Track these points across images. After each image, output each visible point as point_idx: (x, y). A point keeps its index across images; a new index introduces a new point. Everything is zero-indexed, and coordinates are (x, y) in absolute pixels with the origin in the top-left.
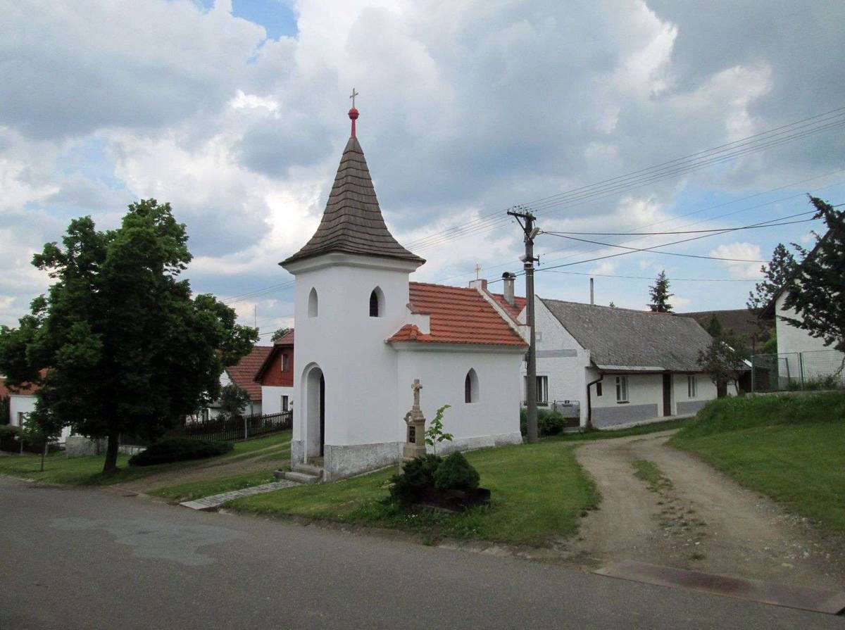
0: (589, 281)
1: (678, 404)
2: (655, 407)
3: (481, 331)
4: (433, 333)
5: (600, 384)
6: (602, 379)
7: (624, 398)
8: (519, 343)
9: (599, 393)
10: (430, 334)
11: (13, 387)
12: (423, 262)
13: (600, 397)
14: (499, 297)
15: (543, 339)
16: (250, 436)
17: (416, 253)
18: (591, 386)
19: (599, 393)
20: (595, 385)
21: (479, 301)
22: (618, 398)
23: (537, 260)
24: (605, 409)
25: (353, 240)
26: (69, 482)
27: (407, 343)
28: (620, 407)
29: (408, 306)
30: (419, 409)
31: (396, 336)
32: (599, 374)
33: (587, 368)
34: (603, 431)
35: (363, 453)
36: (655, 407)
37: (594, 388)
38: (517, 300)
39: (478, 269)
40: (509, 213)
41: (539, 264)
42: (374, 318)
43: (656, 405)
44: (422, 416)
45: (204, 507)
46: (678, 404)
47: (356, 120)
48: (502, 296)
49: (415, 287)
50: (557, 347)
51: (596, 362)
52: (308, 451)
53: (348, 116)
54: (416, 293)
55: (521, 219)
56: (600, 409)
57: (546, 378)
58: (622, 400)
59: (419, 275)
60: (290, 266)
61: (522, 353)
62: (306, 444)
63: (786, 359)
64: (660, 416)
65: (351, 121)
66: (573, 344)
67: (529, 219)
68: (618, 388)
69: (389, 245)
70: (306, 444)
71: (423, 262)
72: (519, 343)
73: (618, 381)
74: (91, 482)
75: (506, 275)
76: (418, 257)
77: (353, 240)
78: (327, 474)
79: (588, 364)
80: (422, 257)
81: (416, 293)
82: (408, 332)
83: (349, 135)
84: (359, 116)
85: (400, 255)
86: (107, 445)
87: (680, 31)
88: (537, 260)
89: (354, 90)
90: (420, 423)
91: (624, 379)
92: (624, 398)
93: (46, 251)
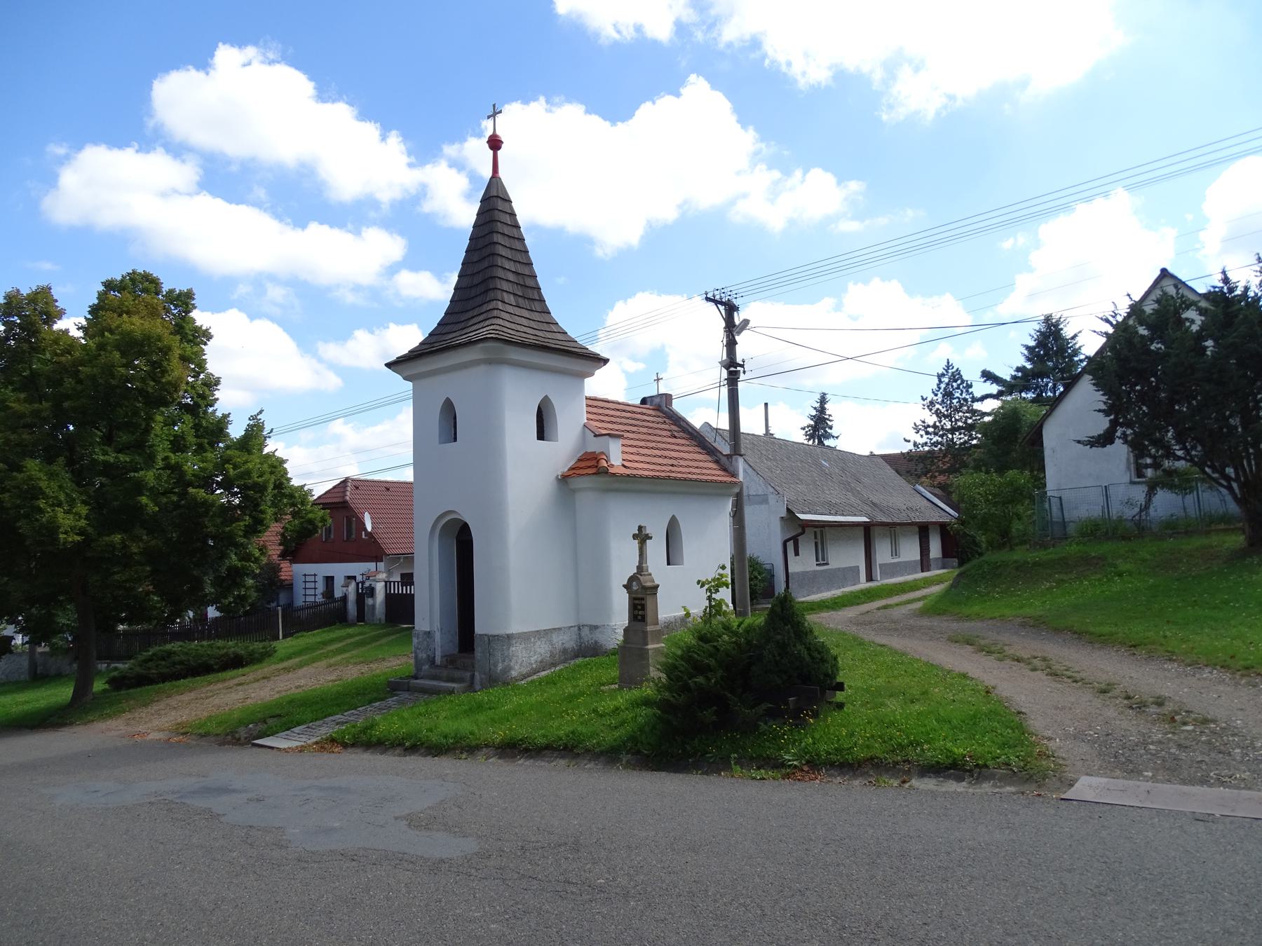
1: (880, 565)
2: (856, 570)
3: (682, 463)
5: (798, 540)
6: (803, 533)
7: (823, 560)
9: (797, 554)
11: (310, 527)
12: (606, 361)
13: (797, 557)
16: (285, 637)
17: (595, 348)
18: (788, 543)
19: (797, 554)
20: (792, 541)
22: (817, 560)
24: (804, 574)
27: (594, 477)
28: (823, 571)
34: (803, 602)
35: (534, 643)
36: (856, 570)
37: (790, 545)
39: (658, 380)
40: (708, 299)
43: (858, 567)
44: (653, 581)
46: (880, 565)
49: (591, 403)
51: (794, 510)
53: (487, 145)
54: (595, 410)
55: (722, 308)
56: (798, 573)
59: (601, 384)
60: (399, 367)
62: (438, 636)
63: (1060, 498)
64: (863, 584)
65: (491, 152)
67: (731, 309)
68: (816, 544)
69: (560, 337)
70: (438, 636)
71: (606, 361)
76: (599, 355)
78: (481, 679)
79: (784, 513)
80: (604, 355)
81: (595, 410)
82: (593, 463)
84: (503, 146)
86: (317, 631)
87: (556, 16)
88: (742, 366)
89: (494, 106)
91: (822, 532)
92: (823, 560)
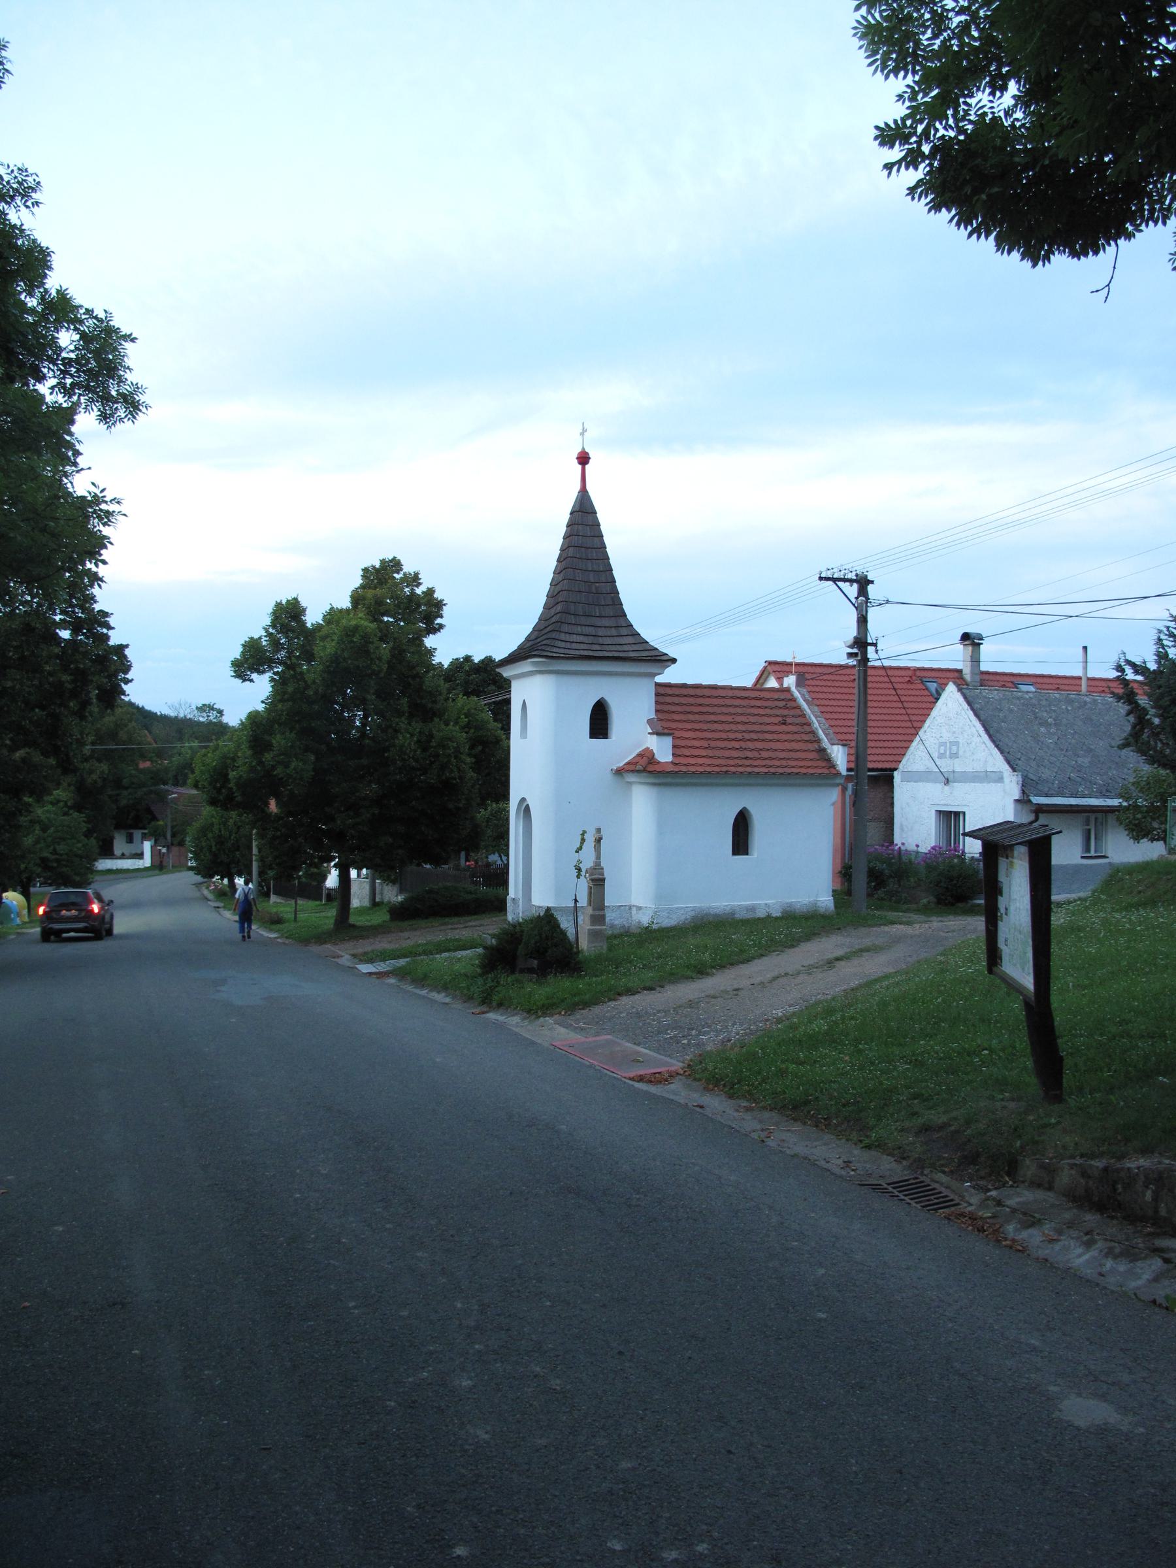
0: (1081, 651)
4: (677, 761)
8: (826, 771)
10: (672, 762)
14: (956, 674)
15: (961, 753)
21: (785, 707)
22: (1088, 850)
23: (875, 645)
25: (568, 638)
26: (822, 966)
29: (650, 722)
30: (600, 865)
31: (628, 764)
32: (1031, 811)
33: (1017, 801)
38: (986, 677)
40: (821, 579)
41: (877, 651)
42: (599, 742)
44: (603, 875)
45: (625, 1000)
47: (587, 466)
48: (960, 671)
50: (979, 767)
52: (523, 912)
57: (964, 813)
58: (1092, 853)
59: (670, 676)
61: (838, 785)
62: (521, 902)
65: (580, 467)
66: (997, 762)
67: (863, 583)
71: (674, 661)
72: (826, 771)
73: (1087, 822)
74: (321, 938)
75: (966, 637)
77: (568, 638)
83: (578, 487)
84: (591, 461)
85: (632, 654)
88: (875, 645)
90: (598, 883)
93: (1015, 99)
